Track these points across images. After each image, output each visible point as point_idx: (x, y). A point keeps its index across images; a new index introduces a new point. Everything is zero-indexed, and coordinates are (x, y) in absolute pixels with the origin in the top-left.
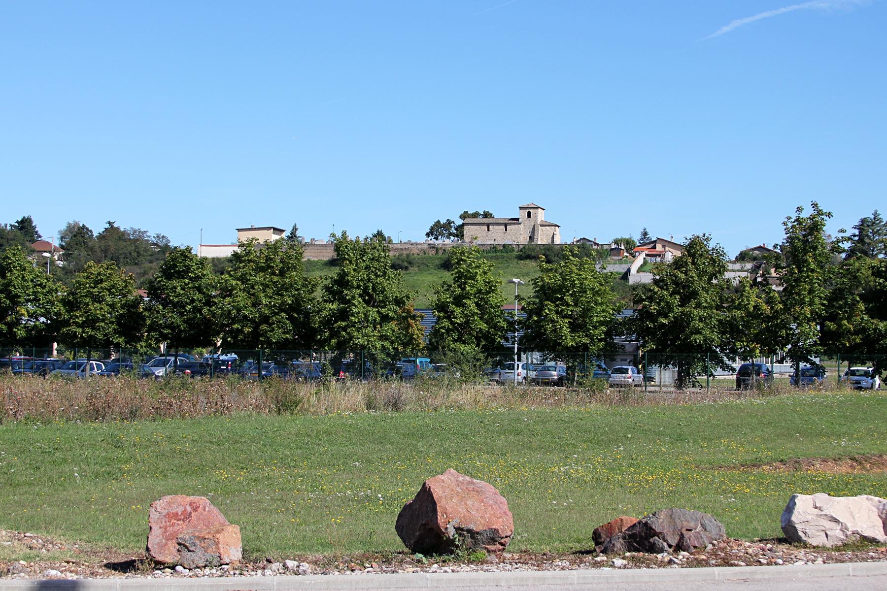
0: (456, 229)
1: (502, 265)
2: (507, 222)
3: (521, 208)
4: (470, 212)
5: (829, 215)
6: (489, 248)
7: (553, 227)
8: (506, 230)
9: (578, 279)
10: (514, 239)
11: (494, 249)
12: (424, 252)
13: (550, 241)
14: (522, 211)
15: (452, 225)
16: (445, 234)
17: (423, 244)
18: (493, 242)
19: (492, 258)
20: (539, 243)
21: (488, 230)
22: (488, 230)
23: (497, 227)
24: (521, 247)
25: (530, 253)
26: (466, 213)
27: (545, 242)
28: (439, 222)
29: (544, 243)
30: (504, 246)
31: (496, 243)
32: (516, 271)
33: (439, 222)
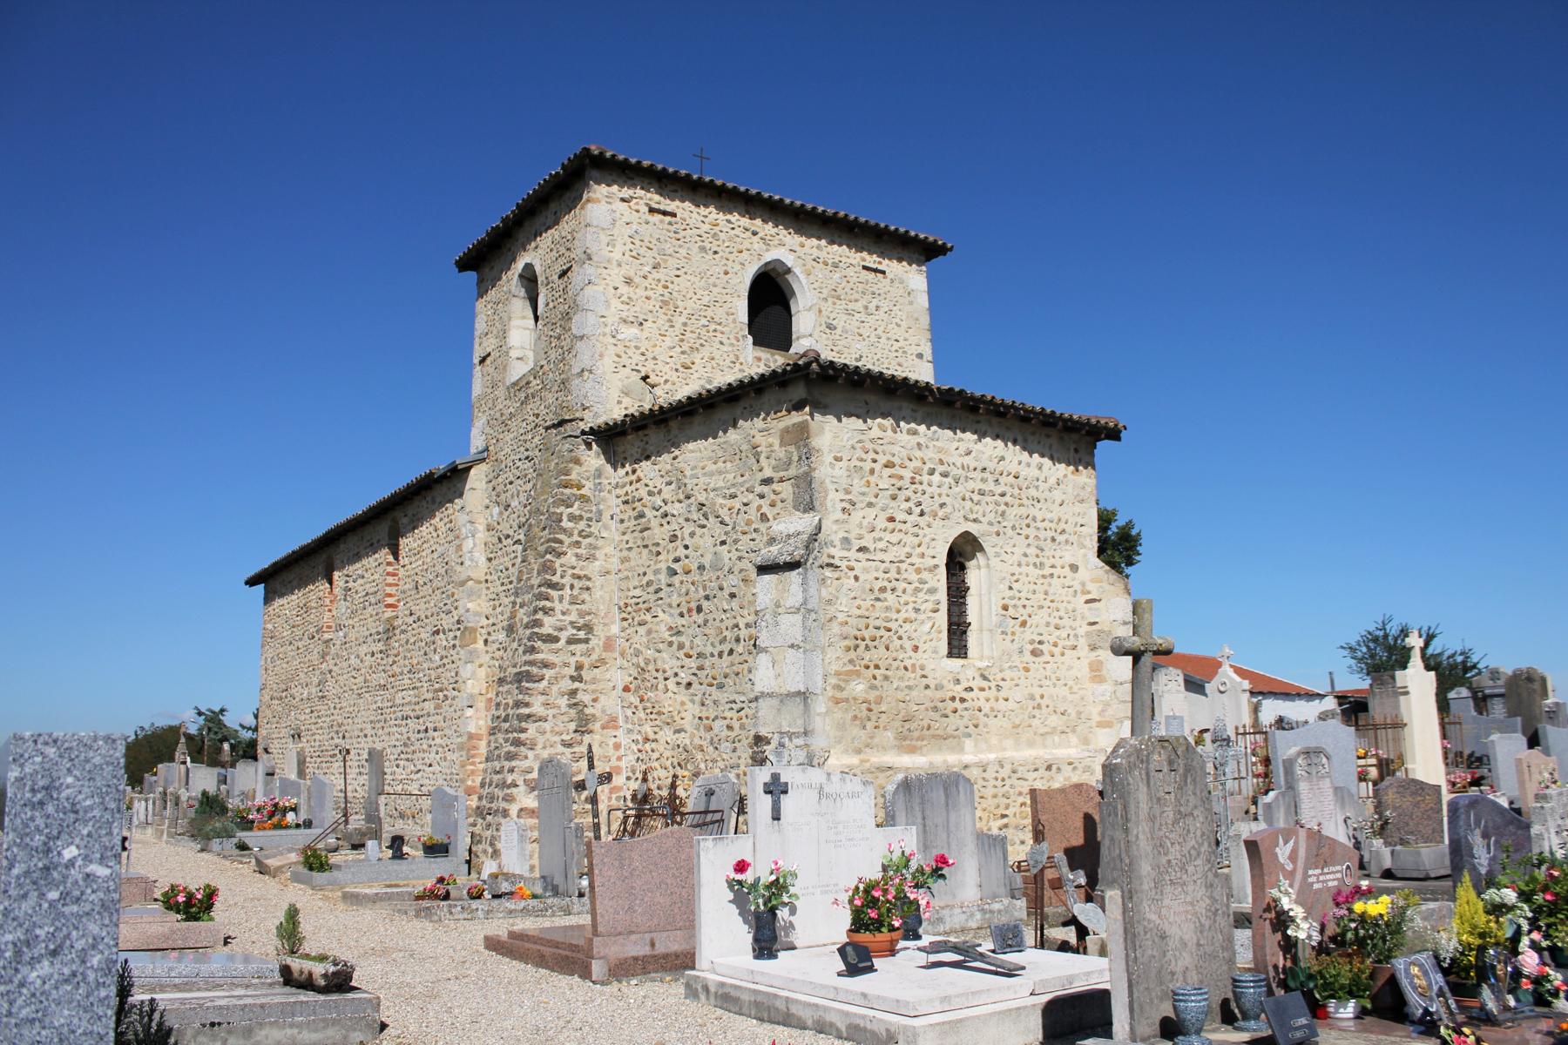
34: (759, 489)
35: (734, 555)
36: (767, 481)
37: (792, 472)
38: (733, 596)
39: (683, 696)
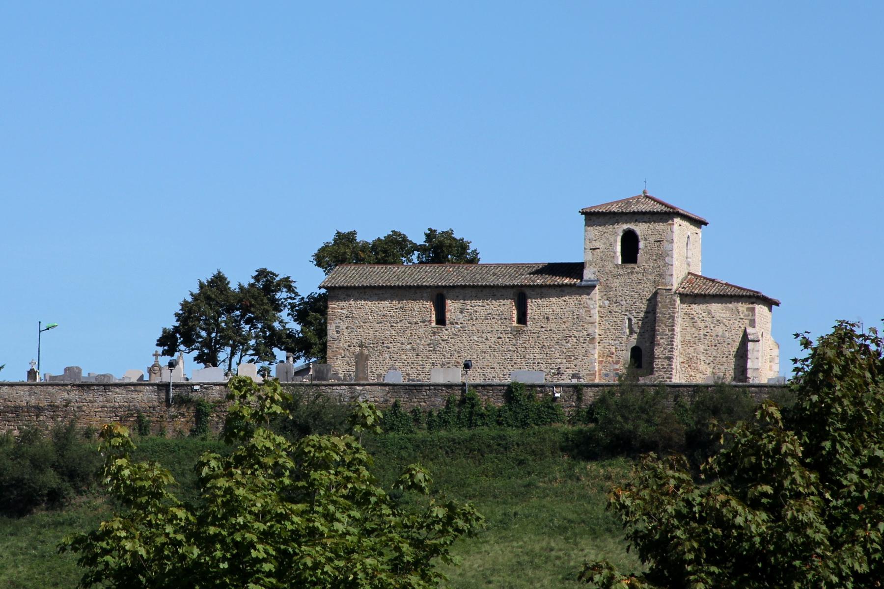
0: (301, 316)
1: (498, 483)
2: (525, 279)
3: (593, 217)
4: (367, 235)
5: (580, 212)
6: (439, 402)
7: (742, 307)
8: (522, 318)
9: (266, 536)
10: (561, 360)
11: (466, 411)
12: (140, 420)
13: (727, 372)
14: (594, 231)
15: (282, 295)
16: (246, 339)
17: (141, 383)
18: (456, 376)
19: (452, 447)
20: (678, 378)
21: (441, 320)
22: (441, 320)
23: (480, 307)
24: (590, 396)
25: (629, 426)
26: (345, 239)
27: (703, 375)
28: (219, 281)
29: (699, 379)
30: (511, 392)
31: (475, 377)
32: (565, 510)
33: (219, 281)
34: (738, 320)
35: (730, 334)
36: (741, 319)
37: (749, 318)
38: (729, 344)
39: (707, 366)
